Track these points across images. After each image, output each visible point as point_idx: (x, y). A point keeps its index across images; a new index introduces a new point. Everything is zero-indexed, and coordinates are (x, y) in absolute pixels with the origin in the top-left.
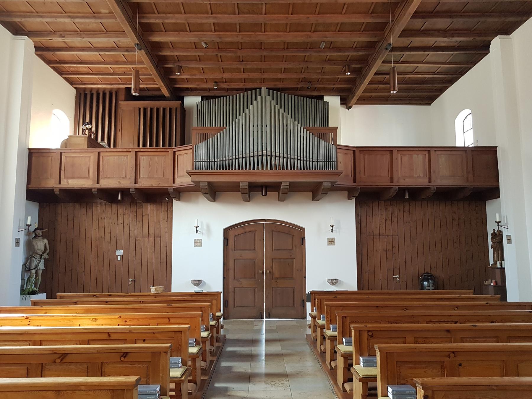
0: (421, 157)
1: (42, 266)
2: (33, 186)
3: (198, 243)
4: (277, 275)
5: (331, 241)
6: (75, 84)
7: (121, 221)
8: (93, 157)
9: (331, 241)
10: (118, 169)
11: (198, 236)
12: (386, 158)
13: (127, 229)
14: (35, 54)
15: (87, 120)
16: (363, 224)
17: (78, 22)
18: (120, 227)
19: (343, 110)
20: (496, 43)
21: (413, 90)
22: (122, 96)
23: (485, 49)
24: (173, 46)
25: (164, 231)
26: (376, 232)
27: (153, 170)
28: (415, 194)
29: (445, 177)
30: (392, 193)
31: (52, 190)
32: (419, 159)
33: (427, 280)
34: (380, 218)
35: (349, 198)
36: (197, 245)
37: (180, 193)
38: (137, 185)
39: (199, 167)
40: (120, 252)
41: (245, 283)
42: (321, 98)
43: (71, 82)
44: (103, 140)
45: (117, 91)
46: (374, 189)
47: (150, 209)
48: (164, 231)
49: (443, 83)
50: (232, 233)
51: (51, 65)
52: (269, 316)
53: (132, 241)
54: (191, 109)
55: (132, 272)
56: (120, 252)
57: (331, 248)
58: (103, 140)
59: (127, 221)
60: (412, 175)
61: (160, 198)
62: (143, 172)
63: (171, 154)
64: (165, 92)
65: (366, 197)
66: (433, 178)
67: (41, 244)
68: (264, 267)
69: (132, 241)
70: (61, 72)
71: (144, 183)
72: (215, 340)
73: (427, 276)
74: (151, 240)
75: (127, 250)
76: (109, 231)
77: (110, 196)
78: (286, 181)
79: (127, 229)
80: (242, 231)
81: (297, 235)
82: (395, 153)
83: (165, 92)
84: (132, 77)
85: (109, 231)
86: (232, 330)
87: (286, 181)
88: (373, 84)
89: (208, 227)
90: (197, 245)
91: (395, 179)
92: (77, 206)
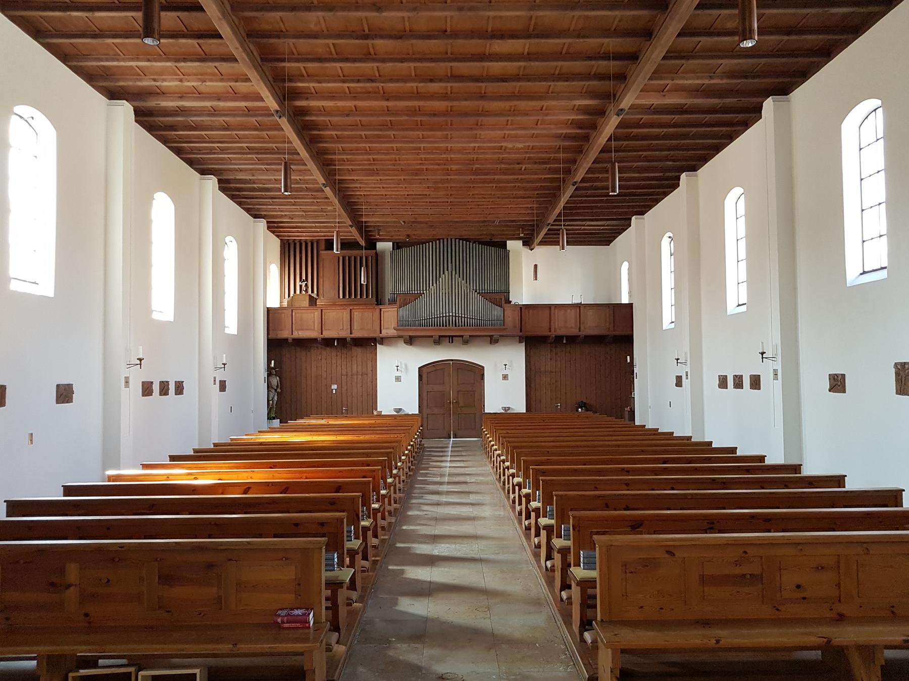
0: (573, 311)
1: (276, 398)
2: (272, 336)
3: (398, 379)
4: (461, 404)
5: (398, 379)
6: (169, 142)
7: (334, 361)
8: (317, 314)
9: (505, 377)
10: (338, 323)
11: (398, 374)
12: (547, 311)
13: (339, 367)
14: (136, 121)
15: (304, 278)
16: (532, 363)
17: (182, 67)
18: (334, 366)
19: (525, 251)
20: (769, 105)
21: (685, 136)
22: (323, 246)
23: (756, 112)
24: (324, 111)
25: (370, 369)
26: (543, 369)
27: (362, 322)
28: (572, 339)
29: (592, 325)
30: (551, 340)
31: (286, 340)
32: (572, 313)
33: (581, 407)
34: (546, 358)
35: (520, 342)
36: (397, 380)
37: (382, 341)
38: (352, 336)
39: (402, 324)
40: (334, 387)
41: (436, 411)
42: (504, 245)
43: (278, 236)
44: (312, 292)
45: (318, 241)
46: (540, 334)
47: (358, 351)
48: (370, 369)
49: (720, 138)
50: (425, 370)
51: (41, 40)
52: (455, 437)
53: (344, 378)
54: (383, 252)
55: (345, 402)
56: (334, 387)
57: (505, 381)
58: (312, 292)
59: (339, 362)
60: (565, 326)
61: (368, 344)
62: (356, 326)
63: (378, 311)
64: (363, 243)
65: (534, 343)
66: (582, 328)
67: (275, 381)
68: (451, 398)
69: (344, 378)
70: (165, 141)
71: (357, 334)
72: (392, 502)
73: (582, 405)
74: (360, 377)
75: (340, 386)
76: (323, 369)
77: (328, 343)
78: (467, 334)
79: (339, 367)
80: (434, 369)
81: (477, 372)
82: (553, 308)
83: (363, 243)
84: (283, 167)
85: (323, 369)
86: (426, 443)
87: (467, 334)
88: (671, 58)
89: (406, 366)
90: (397, 380)
91: (553, 330)
92: (298, 349)
